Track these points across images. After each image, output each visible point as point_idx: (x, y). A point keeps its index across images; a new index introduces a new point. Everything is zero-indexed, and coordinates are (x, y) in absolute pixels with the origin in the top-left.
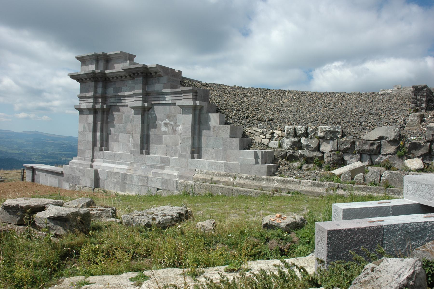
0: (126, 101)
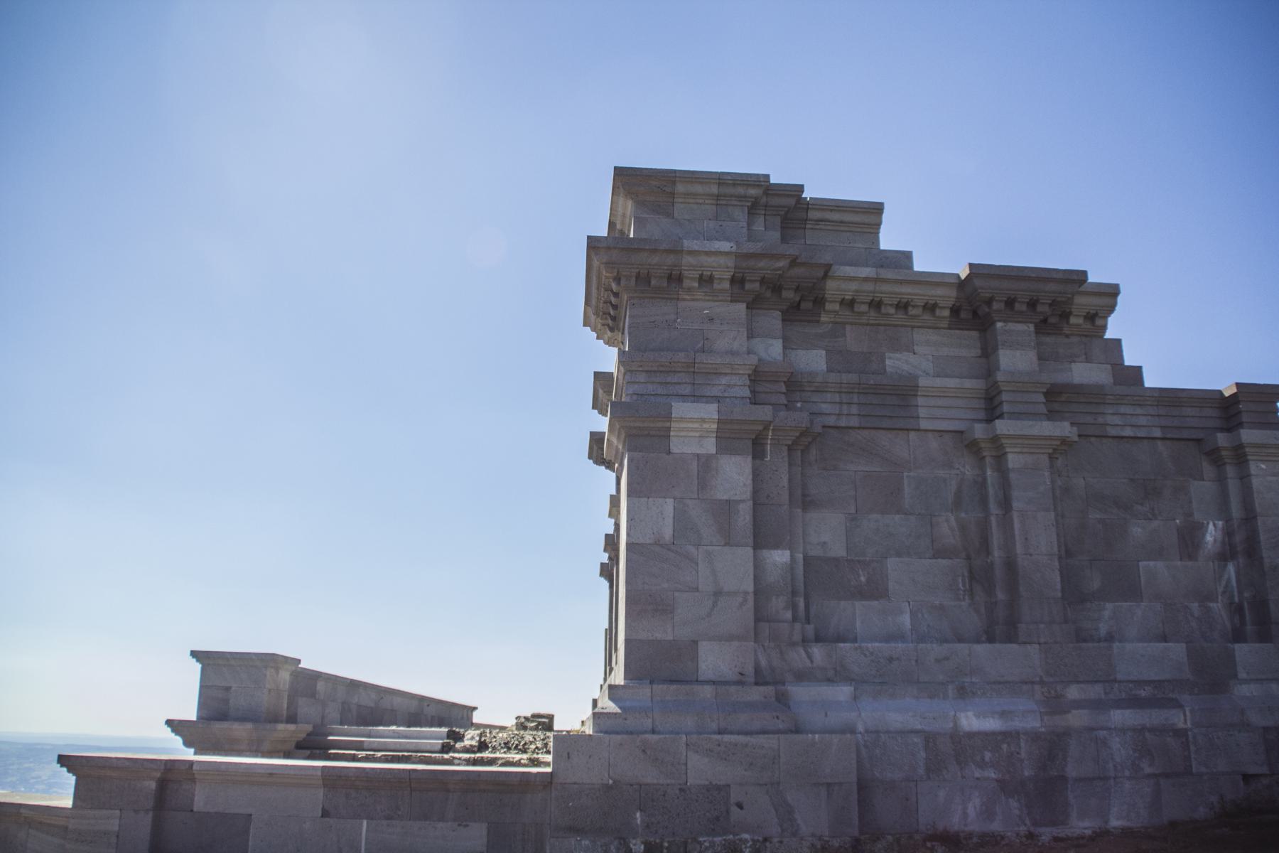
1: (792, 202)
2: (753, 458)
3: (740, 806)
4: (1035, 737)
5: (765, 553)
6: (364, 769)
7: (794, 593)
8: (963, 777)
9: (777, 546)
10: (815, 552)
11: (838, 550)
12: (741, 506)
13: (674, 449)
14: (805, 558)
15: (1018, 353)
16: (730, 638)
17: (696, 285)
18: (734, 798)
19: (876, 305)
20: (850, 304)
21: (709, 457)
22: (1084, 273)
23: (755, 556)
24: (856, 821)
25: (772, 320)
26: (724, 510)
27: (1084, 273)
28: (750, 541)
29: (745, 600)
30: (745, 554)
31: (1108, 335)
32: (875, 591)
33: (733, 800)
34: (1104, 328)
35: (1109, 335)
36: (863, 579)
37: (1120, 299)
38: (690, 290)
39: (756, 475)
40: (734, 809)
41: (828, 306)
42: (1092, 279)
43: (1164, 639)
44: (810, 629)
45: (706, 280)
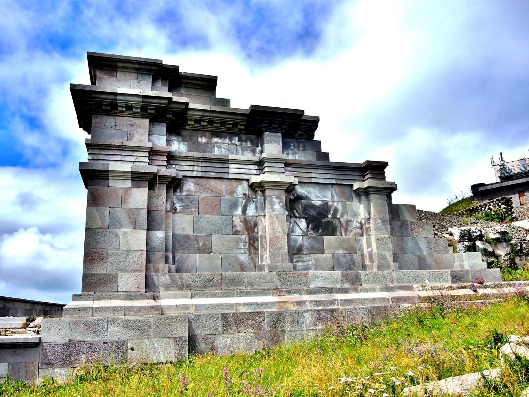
0: (313, 175)
1: (184, 107)
2: (149, 189)
3: (132, 349)
4: (272, 314)
5: (152, 233)
6: (222, 295)
7: (166, 250)
8: (258, 188)
9: (159, 230)
10: (178, 232)
11: (189, 231)
12: (142, 211)
13: (110, 185)
14: (173, 235)
15: (274, 145)
16: (136, 271)
17: (124, 109)
18: (130, 346)
19: (211, 122)
20: (198, 121)
21: (127, 189)
22: (303, 111)
23: (147, 233)
24: (287, 247)
25: (163, 128)
26: (134, 213)
27: (303, 111)
28: (146, 227)
29: (142, 254)
30: (142, 234)
31: (315, 139)
32: (206, 249)
33: (129, 347)
34: (313, 136)
35: (315, 139)
36: (201, 244)
37: (319, 123)
38: (121, 112)
39: (150, 197)
40: (130, 350)
41: (189, 123)
42: (306, 114)
43: (333, 269)
44: (173, 267)
45: (129, 107)
